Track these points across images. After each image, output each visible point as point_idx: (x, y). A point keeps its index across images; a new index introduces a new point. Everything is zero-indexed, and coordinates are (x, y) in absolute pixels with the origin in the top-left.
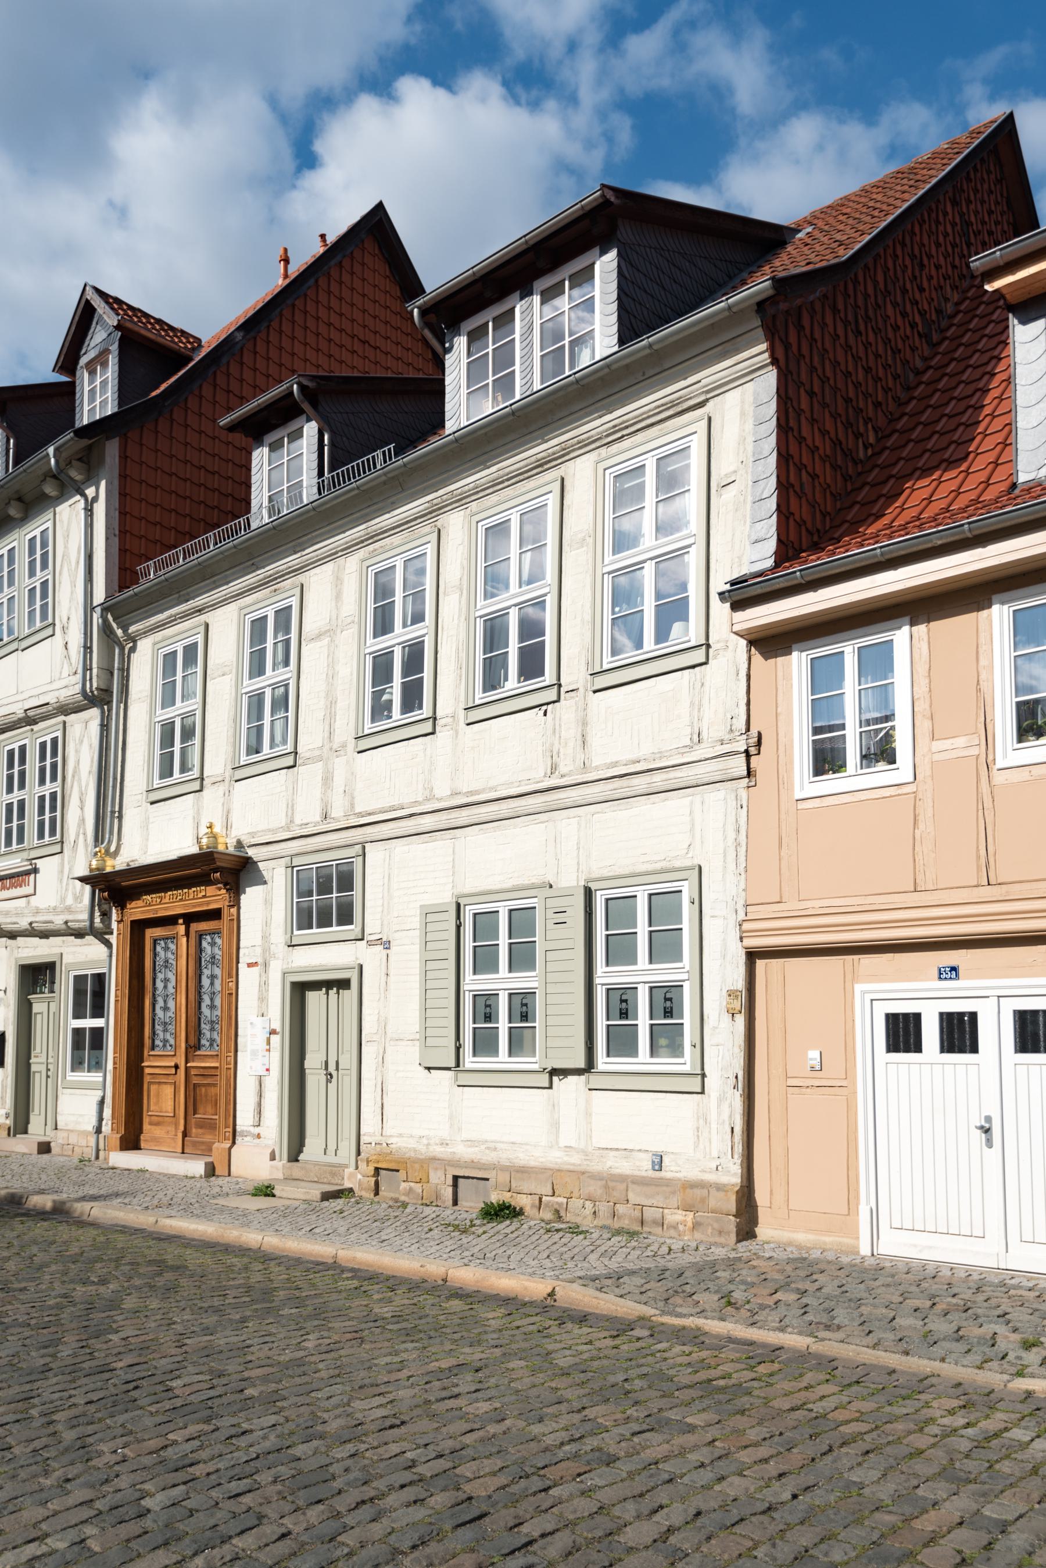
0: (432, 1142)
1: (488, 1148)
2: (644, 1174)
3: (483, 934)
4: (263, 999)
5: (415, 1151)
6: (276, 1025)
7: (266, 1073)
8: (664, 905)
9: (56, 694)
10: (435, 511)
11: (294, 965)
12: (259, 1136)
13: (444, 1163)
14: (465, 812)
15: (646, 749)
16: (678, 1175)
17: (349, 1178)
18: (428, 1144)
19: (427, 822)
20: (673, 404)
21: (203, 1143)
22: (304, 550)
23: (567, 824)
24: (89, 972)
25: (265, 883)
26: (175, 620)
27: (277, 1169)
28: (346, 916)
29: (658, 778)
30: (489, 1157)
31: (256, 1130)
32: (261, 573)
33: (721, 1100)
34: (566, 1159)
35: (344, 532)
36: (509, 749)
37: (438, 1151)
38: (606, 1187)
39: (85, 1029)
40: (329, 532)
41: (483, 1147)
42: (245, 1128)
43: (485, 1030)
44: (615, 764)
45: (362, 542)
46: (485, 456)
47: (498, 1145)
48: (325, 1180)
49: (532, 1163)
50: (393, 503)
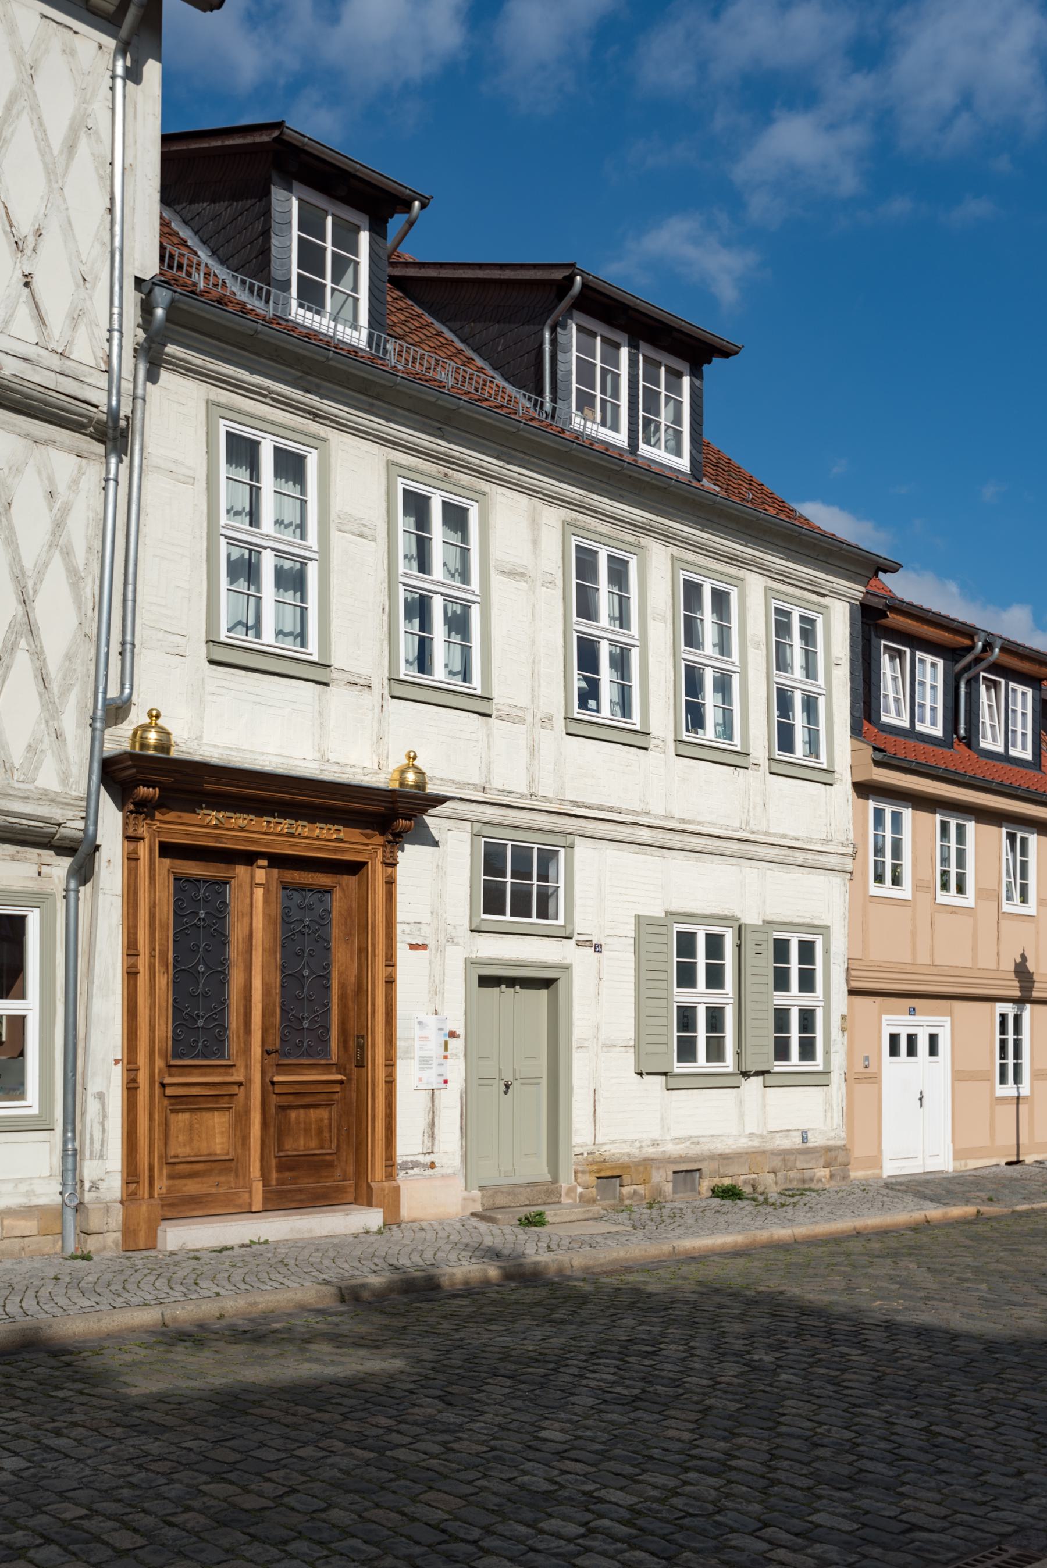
0: (644, 1144)
1: (692, 1143)
2: (797, 1147)
3: (691, 952)
5: (629, 1155)
7: (443, 1086)
8: (807, 950)
11: (480, 955)
12: (432, 1165)
14: (678, 837)
16: (816, 1144)
17: (567, 1194)
18: (641, 1147)
19: (645, 835)
21: (300, 1190)
22: (509, 463)
23: (750, 872)
25: (436, 844)
26: (265, 396)
27: (474, 1200)
28: (493, 902)
29: (810, 856)
30: (694, 1151)
31: (428, 1159)
32: (442, 446)
33: (839, 1088)
34: (750, 1143)
35: (560, 481)
36: (708, 795)
37: (650, 1151)
38: (784, 1160)
40: (549, 470)
41: (688, 1143)
43: (687, 1042)
44: (784, 836)
45: (569, 503)
46: (709, 523)
47: (701, 1140)
48: (540, 1201)
49: (727, 1151)
50: (621, 496)
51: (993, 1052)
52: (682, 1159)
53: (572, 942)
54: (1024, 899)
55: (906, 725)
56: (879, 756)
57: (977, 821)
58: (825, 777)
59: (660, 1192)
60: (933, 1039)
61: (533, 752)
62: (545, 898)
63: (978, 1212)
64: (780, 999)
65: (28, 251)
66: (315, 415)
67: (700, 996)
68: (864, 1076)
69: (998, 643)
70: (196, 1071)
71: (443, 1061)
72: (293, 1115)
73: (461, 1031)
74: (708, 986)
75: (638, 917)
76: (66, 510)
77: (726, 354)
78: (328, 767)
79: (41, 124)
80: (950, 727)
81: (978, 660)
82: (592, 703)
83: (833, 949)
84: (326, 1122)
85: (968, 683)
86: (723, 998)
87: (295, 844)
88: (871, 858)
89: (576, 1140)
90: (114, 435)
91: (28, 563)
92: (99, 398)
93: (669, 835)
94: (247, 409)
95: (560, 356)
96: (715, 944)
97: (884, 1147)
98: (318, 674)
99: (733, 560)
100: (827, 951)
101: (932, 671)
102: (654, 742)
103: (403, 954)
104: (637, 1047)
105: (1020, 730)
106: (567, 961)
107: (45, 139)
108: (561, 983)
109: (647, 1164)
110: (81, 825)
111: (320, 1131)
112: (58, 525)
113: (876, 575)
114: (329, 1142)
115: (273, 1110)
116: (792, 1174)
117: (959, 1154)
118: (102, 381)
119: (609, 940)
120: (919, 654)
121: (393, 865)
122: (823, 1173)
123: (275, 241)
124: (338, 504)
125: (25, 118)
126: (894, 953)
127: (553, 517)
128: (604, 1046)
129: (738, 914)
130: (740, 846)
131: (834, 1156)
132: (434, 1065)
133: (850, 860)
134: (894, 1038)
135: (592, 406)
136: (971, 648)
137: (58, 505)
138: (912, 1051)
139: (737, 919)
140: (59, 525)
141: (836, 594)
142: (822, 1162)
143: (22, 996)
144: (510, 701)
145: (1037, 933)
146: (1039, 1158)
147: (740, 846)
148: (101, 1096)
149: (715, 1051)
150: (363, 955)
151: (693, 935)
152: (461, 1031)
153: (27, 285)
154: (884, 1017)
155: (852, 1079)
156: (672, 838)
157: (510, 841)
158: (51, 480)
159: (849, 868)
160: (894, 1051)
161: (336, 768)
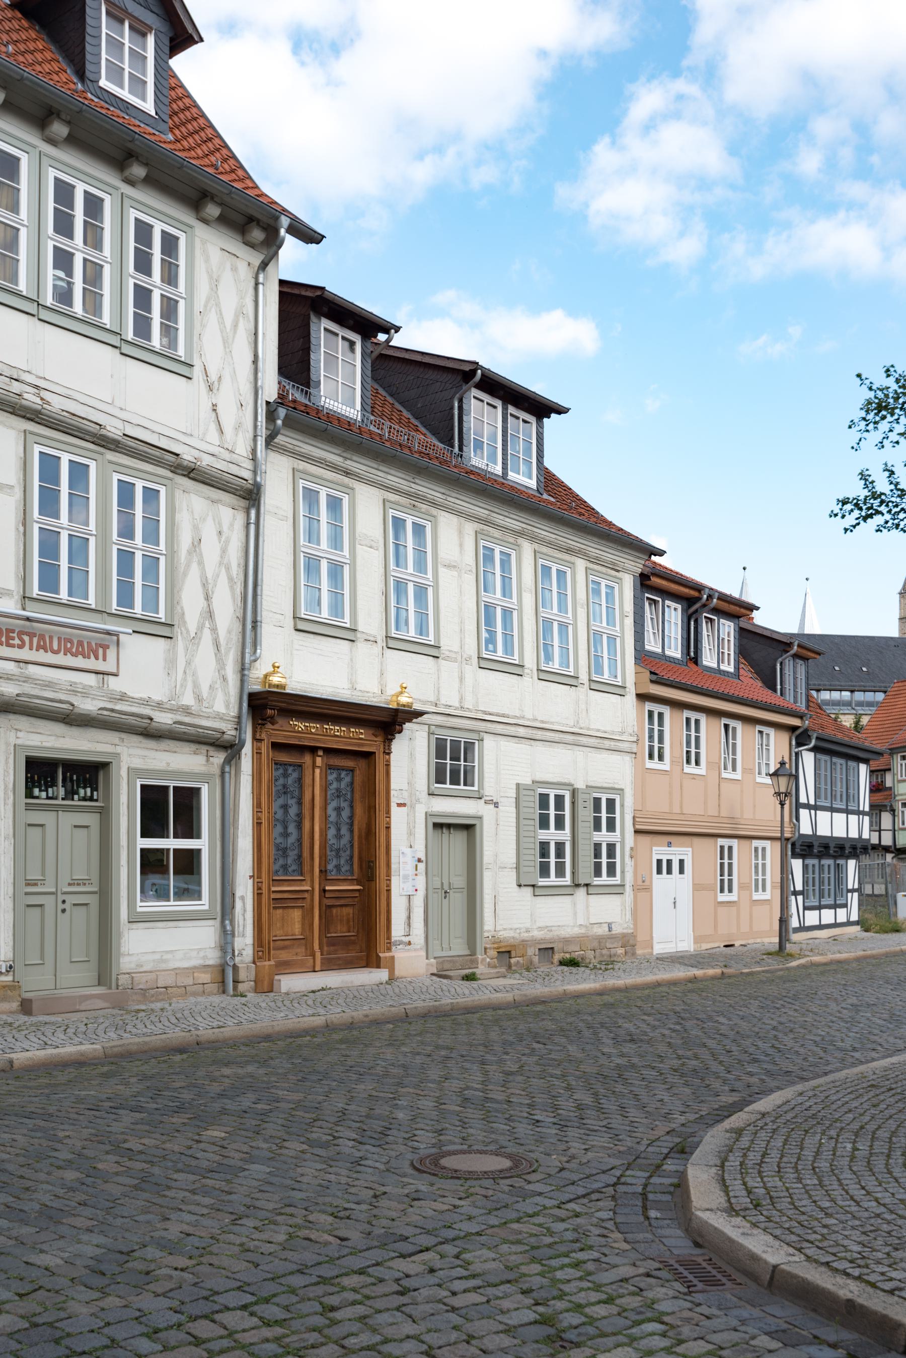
3: (546, 806)
4: (411, 833)
6: (422, 856)
7: (414, 893)
8: (611, 803)
9: (196, 454)
10: (520, 534)
11: (434, 810)
12: (409, 943)
13: (535, 942)
15: (608, 729)
19: (522, 731)
20: (614, 564)
21: (339, 958)
23: (580, 754)
24: (172, 784)
27: (432, 966)
29: (612, 743)
30: (549, 936)
31: (406, 939)
36: (556, 705)
37: (525, 936)
38: (599, 942)
39: (168, 850)
42: (397, 939)
43: (543, 865)
44: (598, 730)
47: (553, 928)
49: (567, 936)
51: (716, 871)
52: (543, 941)
53: (482, 801)
54: (734, 769)
55: (659, 650)
56: (654, 678)
57: (707, 716)
58: (619, 690)
59: (531, 962)
60: (681, 862)
61: (461, 679)
62: (469, 772)
63: (723, 973)
64: (543, 835)
65: (215, 391)
66: (347, 473)
67: (552, 835)
68: (643, 888)
69: (717, 595)
70: (286, 883)
71: (415, 877)
72: (334, 911)
73: (423, 858)
74: (556, 829)
75: (518, 785)
76: (227, 541)
77: (559, 412)
78: (355, 693)
79: (221, 314)
80: (685, 652)
81: (704, 606)
82: (491, 647)
83: (626, 804)
84: (351, 915)
85: (696, 621)
86: (569, 836)
87: (339, 742)
88: (647, 743)
89: (486, 928)
90: (251, 496)
91: (209, 575)
92: (247, 475)
93: (535, 731)
94: (315, 473)
95: (465, 418)
96: (559, 800)
97: (654, 935)
98: (349, 634)
99: (569, 551)
100: (622, 806)
101: (674, 613)
102: (526, 671)
103: (394, 809)
104: (518, 868)
105: (726, 652)
106: (480, 814)
107: (223, 323)
108: (478, 828)
109: (524, 943)
110: (233, 733)
111: (348, 921)
112: (224, 552)
113: (650, 557)
114: (355, 926)
115: (324, 908)
116: (605, 952)
117: (697, 940)
118: (249, 465)
119: (502, 800)
120: (667, 602)
121: (389, 754)
122: (621, 951)
123: (312, 356)
124: (360, 528)
125: (213, 310)
126: (662, 808)
127: (470, 528)
128: (500, 868)
129: (572, 782)
130: (573, 738)
131: (628, 942)
132: (410, 880)
133: (635, 745)
134: (659, 862)
135: (482, 449)
136: (699, 599)
137: (223, 539)
138: (669, 871)
139: (572, 785)
140: (224, 551)
141: (626, 571)
142: (620, 945)
143: (199, 836)
144: (449, 648)
145: (742, 791)
146: (743, 943)
147: (573, 738)
148: (242, 898)
149: (560, 872)
150: (372, 811)
151: (548, 795)
152: (423, 858)
153: (215, 410)
154: (654, 848)
155: (636, 889)
156: (537, 733)
157: (449, 736)
158: (220, 524)
159: (635, 750)
160: (659, 871)
161: (359, 694)
